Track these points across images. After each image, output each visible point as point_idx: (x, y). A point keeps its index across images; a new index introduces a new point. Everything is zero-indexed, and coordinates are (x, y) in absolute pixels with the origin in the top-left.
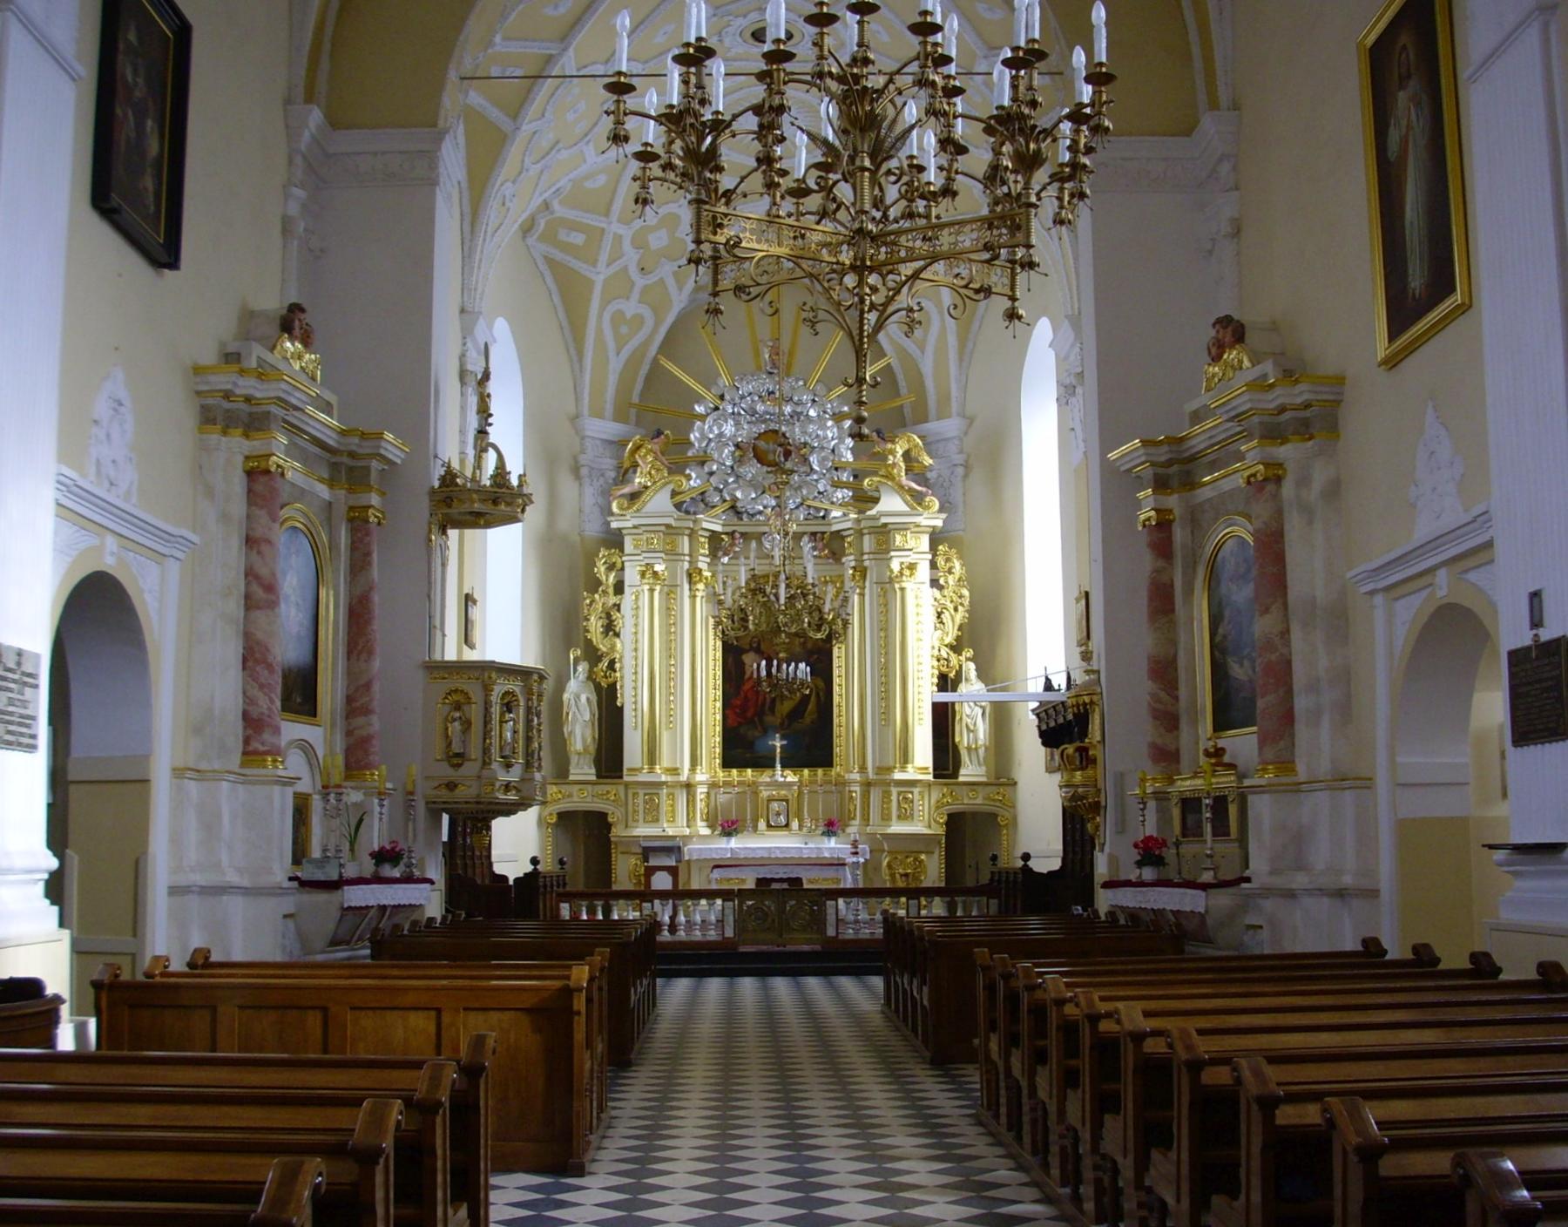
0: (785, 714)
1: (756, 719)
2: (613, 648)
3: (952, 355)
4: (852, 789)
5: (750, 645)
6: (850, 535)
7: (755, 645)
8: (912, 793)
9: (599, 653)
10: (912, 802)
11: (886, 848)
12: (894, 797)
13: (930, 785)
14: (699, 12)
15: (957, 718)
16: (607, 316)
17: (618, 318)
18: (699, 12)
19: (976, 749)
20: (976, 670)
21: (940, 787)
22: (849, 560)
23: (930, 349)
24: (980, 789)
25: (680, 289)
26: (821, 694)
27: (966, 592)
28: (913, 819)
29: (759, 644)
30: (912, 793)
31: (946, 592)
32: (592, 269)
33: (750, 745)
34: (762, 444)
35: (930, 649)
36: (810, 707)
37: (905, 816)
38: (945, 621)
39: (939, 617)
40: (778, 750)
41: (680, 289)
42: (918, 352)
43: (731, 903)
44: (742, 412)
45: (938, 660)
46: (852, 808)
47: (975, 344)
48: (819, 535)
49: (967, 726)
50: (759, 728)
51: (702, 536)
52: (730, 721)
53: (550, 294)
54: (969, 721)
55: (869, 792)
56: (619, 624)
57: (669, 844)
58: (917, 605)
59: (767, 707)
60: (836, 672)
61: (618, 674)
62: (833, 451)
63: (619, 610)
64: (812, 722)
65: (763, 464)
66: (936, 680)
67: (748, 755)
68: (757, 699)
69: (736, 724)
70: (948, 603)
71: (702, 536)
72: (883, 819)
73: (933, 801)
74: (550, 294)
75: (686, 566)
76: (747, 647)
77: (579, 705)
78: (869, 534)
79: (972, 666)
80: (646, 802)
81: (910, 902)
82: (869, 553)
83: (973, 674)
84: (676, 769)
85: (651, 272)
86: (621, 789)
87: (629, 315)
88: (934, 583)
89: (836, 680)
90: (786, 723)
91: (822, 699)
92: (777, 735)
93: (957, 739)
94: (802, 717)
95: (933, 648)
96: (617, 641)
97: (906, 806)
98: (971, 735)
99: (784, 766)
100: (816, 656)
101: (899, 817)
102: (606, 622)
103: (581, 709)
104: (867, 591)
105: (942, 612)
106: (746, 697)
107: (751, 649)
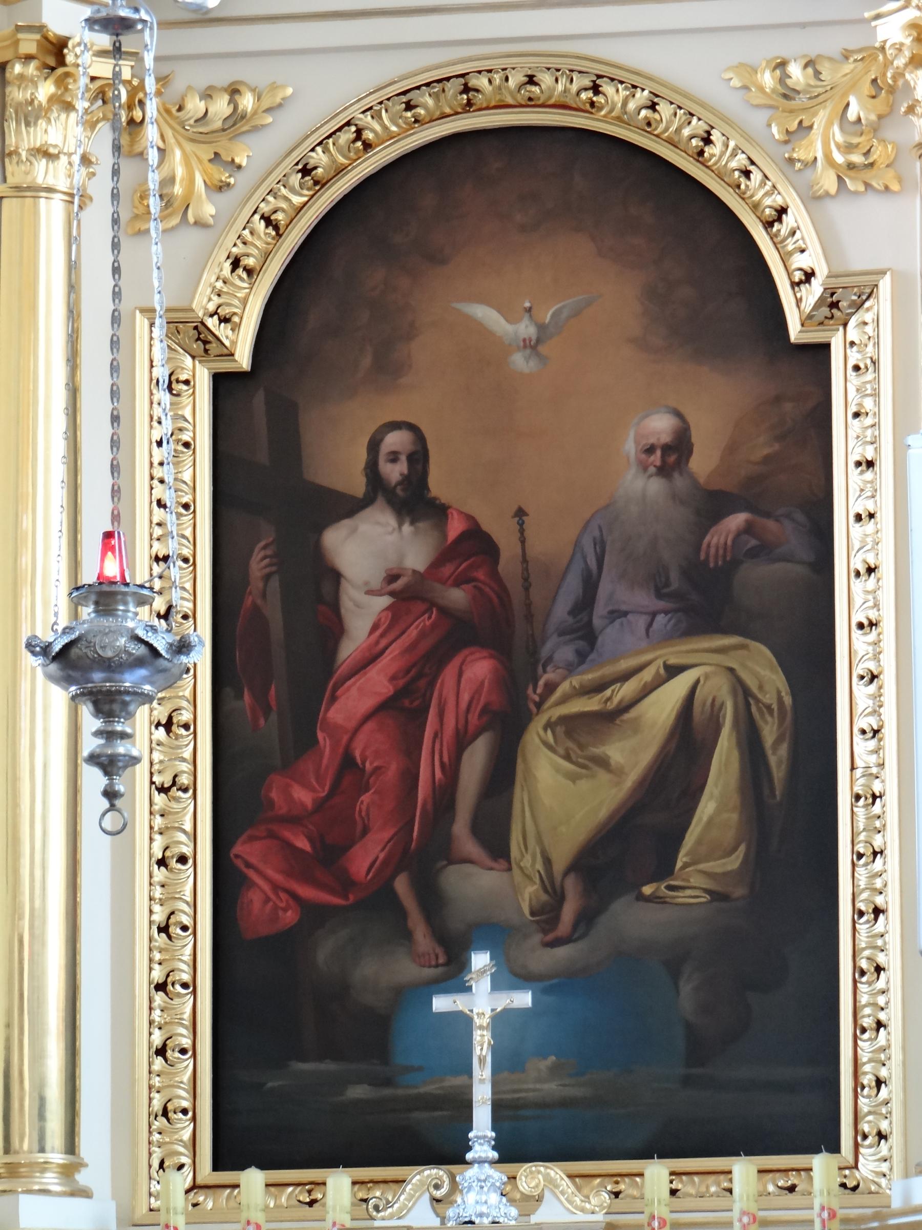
0: (562, 858)
1: (402, 885)
5: (372, 469)
7: (394, 472)
14: (524, 1188)
18: (524, 1188)
26: (769, 732)
36: (707, 808)
58: (248, 1223)
59: (461, 827)
64: (716, 896)
67: (358, 1092)
68: (410, 778)
69: (290, 917)
76: (358, 485)
90: (568, 912)
92: (441, 1003)
106: (348, 763)
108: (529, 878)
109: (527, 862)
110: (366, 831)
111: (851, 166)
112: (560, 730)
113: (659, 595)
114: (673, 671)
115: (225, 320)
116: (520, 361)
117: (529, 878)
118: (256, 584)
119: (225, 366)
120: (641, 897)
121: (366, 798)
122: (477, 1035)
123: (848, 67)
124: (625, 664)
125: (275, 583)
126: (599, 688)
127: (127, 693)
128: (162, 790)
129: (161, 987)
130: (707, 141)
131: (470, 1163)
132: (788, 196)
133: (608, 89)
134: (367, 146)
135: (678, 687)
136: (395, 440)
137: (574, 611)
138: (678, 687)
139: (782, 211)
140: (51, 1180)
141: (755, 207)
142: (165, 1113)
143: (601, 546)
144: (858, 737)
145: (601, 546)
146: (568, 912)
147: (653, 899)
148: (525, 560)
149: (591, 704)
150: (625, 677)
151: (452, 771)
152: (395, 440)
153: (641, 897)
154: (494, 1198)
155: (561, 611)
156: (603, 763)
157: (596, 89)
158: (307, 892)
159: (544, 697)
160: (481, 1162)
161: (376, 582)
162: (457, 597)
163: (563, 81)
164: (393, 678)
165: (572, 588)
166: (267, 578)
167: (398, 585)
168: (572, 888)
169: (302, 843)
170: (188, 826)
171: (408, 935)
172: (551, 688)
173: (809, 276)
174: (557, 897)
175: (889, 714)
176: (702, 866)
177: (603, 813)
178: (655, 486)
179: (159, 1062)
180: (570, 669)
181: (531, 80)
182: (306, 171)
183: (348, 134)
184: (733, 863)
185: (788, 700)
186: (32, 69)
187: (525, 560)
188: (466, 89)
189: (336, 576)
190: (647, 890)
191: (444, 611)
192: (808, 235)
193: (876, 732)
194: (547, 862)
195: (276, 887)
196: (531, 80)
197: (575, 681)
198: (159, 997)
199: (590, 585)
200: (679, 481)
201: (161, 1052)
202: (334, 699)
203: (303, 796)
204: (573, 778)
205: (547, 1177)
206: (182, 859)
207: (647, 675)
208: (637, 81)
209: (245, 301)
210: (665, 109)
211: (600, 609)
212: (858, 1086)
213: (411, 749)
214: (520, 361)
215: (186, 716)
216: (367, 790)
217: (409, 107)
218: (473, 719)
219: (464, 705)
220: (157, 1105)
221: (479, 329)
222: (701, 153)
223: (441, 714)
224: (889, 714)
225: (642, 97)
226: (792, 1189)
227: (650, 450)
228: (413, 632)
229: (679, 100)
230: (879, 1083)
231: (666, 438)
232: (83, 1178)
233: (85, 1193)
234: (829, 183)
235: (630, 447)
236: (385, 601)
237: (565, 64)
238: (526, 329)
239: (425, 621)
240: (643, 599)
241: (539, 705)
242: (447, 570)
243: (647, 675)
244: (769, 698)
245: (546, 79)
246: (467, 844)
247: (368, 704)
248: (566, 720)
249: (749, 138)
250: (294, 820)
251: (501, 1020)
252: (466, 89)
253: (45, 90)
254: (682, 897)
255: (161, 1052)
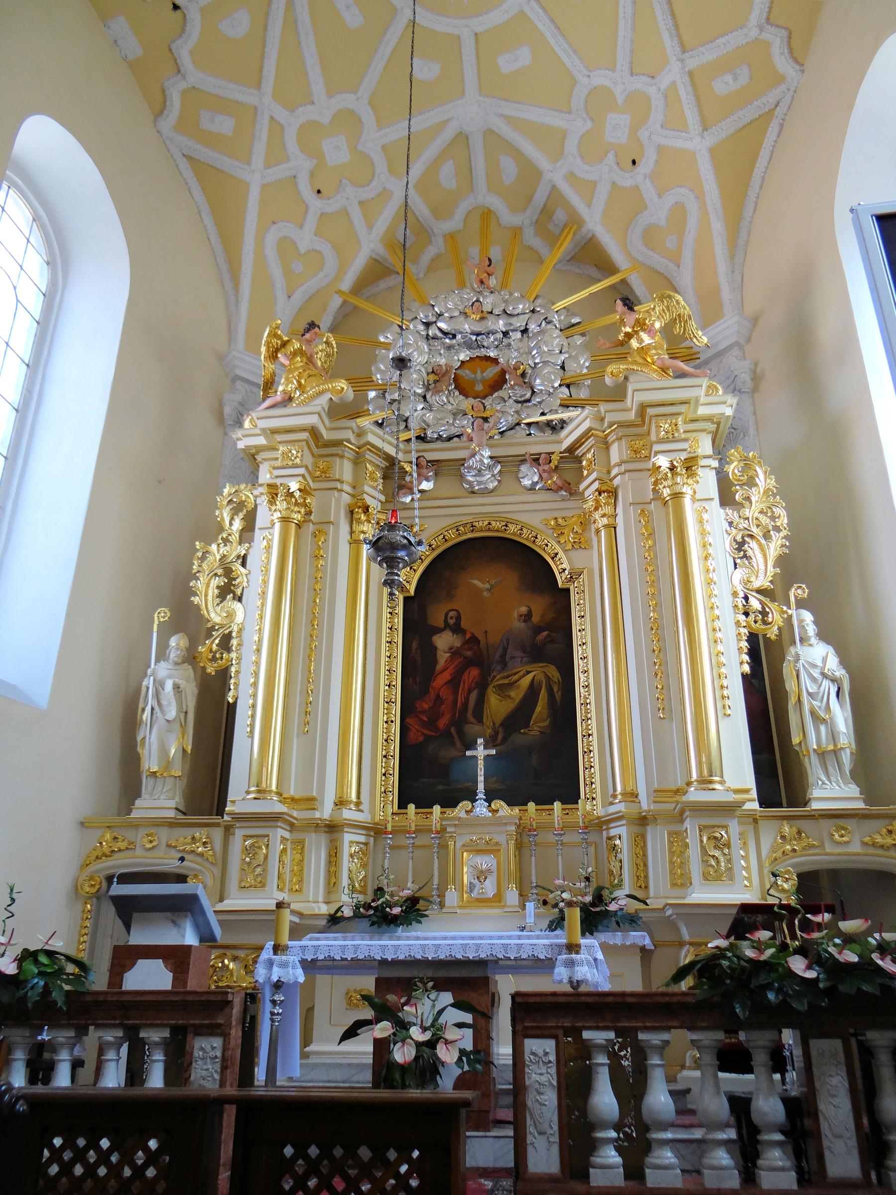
0: (498, 722)
1: (453, 730)
2: (231, 615)
3: (720, 248)
4: (613, 832)
5: (446, 621)
6: (589, 450)
8: (725, 827)
9: (209, 625)
10: (728, 845)
11: (686, 937)
12: (692, 840)
13: (755, 821)
15: (792, 700)
16: (271, 239)
17: (286, 247)
19: (836, 752)
20: (815, 622)
21: (776, 823)
22: (589, 486)
23: (687, 256)
24: (850, 824)
25: (370, 227)
26: (555, 689)
27: (780, 511)
28: (731, 878)
29: (458, 618)
30: (725, 827)
31: (747, 512)
32: (245, 166)
33: (443, 771)
34: (466, 373)
35: (731, 598)
36: (539, 709)
37: (712, 876)
38: (750, 553)
39: (739, 549)
40: (481, 764)
41: (370, 227)
42: (672, 266)
43: (217, 1042)
44: (440, 335)
45: (746, 614)
46: (614, 866)
47: (749, 232)
48: (543, 456)
49: (813, 713)
50: (458, 743)
51: (371, 462)
52: (412, 735)
53: (199, 212)
54: (816, 703)
55: (643, 837)
56: (242, 581)
57: (496, 1004)
59: (469, 714)
60: (577, 652)
61: (233, 655)
62: (563, 368)
63: (244, 564)
65: (466, 396)
66: (745, 644)
67: (440, 787)
68: (455, 701)
69: (421, 739)
70: (755, 530)
71: (371, 462)
72: (674, 885)
73: (765, 851)
74: (199, 212)
75: (346, 499)
76: (442, 625)
77: (162, 697)
78: (619, 439)
79: (807, 616)
80: (247, 850)
81: (816, 1045)
82: (619, 465)
83: (811, 630)
84: (313, 799)
85: (328, 199)
86: (217, 834)
87: (303, 247)
88: (726, 498)
89: (578, 665)
90: (500, 737)
91: (558, 696)
93: (796, 740)
94: (527, 725)
95: (735, 594)
96: (237, 606)
97: (717, 853)
98: (823, 728)
99: (490, 797)
100: (546, 633)
101: (706, 877)
102: (221, 581)
103: (164, 702)
104: (620, 520)
105: (743, 543)
107: (447, 626)
108: (488, 727)
109: (488, 723)
110: (443, 715)
111: (574, 542)
112: (497, 688)
113: (524, 652)
114: (528, 672)
115: (407, 582)
116: (485, 594)
117: (488, 727)
118: (414, 651)
119: (407, 595)
120: (520, 733)
121: (443, 706)
122: (479, 762)
123: (574, 519)
124: (514, 671)
125: (419, 650)
126: (508, 677)
127: (399, 558)
128: (387, 702)
129: (385, 756)
130: (536, 538)
131: (477, 800)
132: (558, 549)
133: (510, 525)
134: (446, 540)
135: (530, 676)
136: (452, 614)
137: (501, 656)
138: (530, 676)
139: (557, 554)
140: (352, 807)
141: (549, 554)
142: (385, 792)
143: (508, 641)
144: (581, 688)
145: (508, 641)
146: (500, 737)
147: (524, 733)
148: (487, 644)
149: (506, 681)
150: (515, 674)
151: (467, 700)
152: (452, 614)
153: (520, 733)
154: (485, 810)
155: (497, 657)
156: (509, 697)
157: (506, 526)
158: (426, 732)
159: (492, 680)
160: (481, 799)
161: (446, 649)
162: (469, 653)
163: (498, 523)
164: (451, 675)
165: (500, 650)
166: (417, 649)
167: (452, 650)
168: (500, 730)
169: (425, 719)
170: (394, 713)
171: (454, 744)
172: (494, 677)
173: (564, 570)
174: (497, 733)
175: (591, 681)
176: (538, 724)
177: (509, 710)
178: (523, 625)
179: (383, 778)
180: (500, 672)
181: (489, 524)
182: (430, 546)
183: (442, 536)
184: (547, 723)
185: (560, 680)
186: (360, 510)
187: (487, 644)
188: (472, 526)
189: (436, 648)
190: (522, 731)
191: (465, 658)
192: (564, 559)
193: (587, 686)
194: (494, 724)
195: (418, 731)
196: (489, 524)
197: (501, 675)
198: (384, 760)
199: (505, 650)
200: (529, 624)
201: (384, 775)
202: (434, 680)
203: (426, 706)
204: (501, 701)
205: (500, 804)
206: (392, 722)
207: (521, 674)
208: (517, 523)
209: (413, 578)
210: (525, 530)
211: (508, 656)
212: (585, 785)
213: (456, 693)
214: (485, 594)
215: (394, 683)
216: (443, 704)
217: (457, 530)
218: (473, 685)
219: (470, 681)
220: (383, 789)
221: (475, 587)
222: (534, 541)
223: (464, 683)
224: (591, 681)
225: (519, 527)
226: (568, 814)
227: (521, 616)
228: (456, 663)
229: (528, 527)
230: (592, 783)
231: (525, 613)
232: (361, 807)
233: (362, 811)
234: (569, 547)
235: (516, 615)
236: (449, 655)
237: (498, 519)
238: (487, 586)
239: (460, 660)
240: (519, 654)
241: (491, 681)
242: (466, 646)
243: (521, 674)
244: (555, 679)
245: (493, 523)
246: (472, 719)
247: (444, 681)
248: (499, 685)
249: (547, 535)
250: (422, 712)
251: (487, 758)
252: (472, 526)
253: (363, 517)
254: (532, 733)
255: (384, 775)
